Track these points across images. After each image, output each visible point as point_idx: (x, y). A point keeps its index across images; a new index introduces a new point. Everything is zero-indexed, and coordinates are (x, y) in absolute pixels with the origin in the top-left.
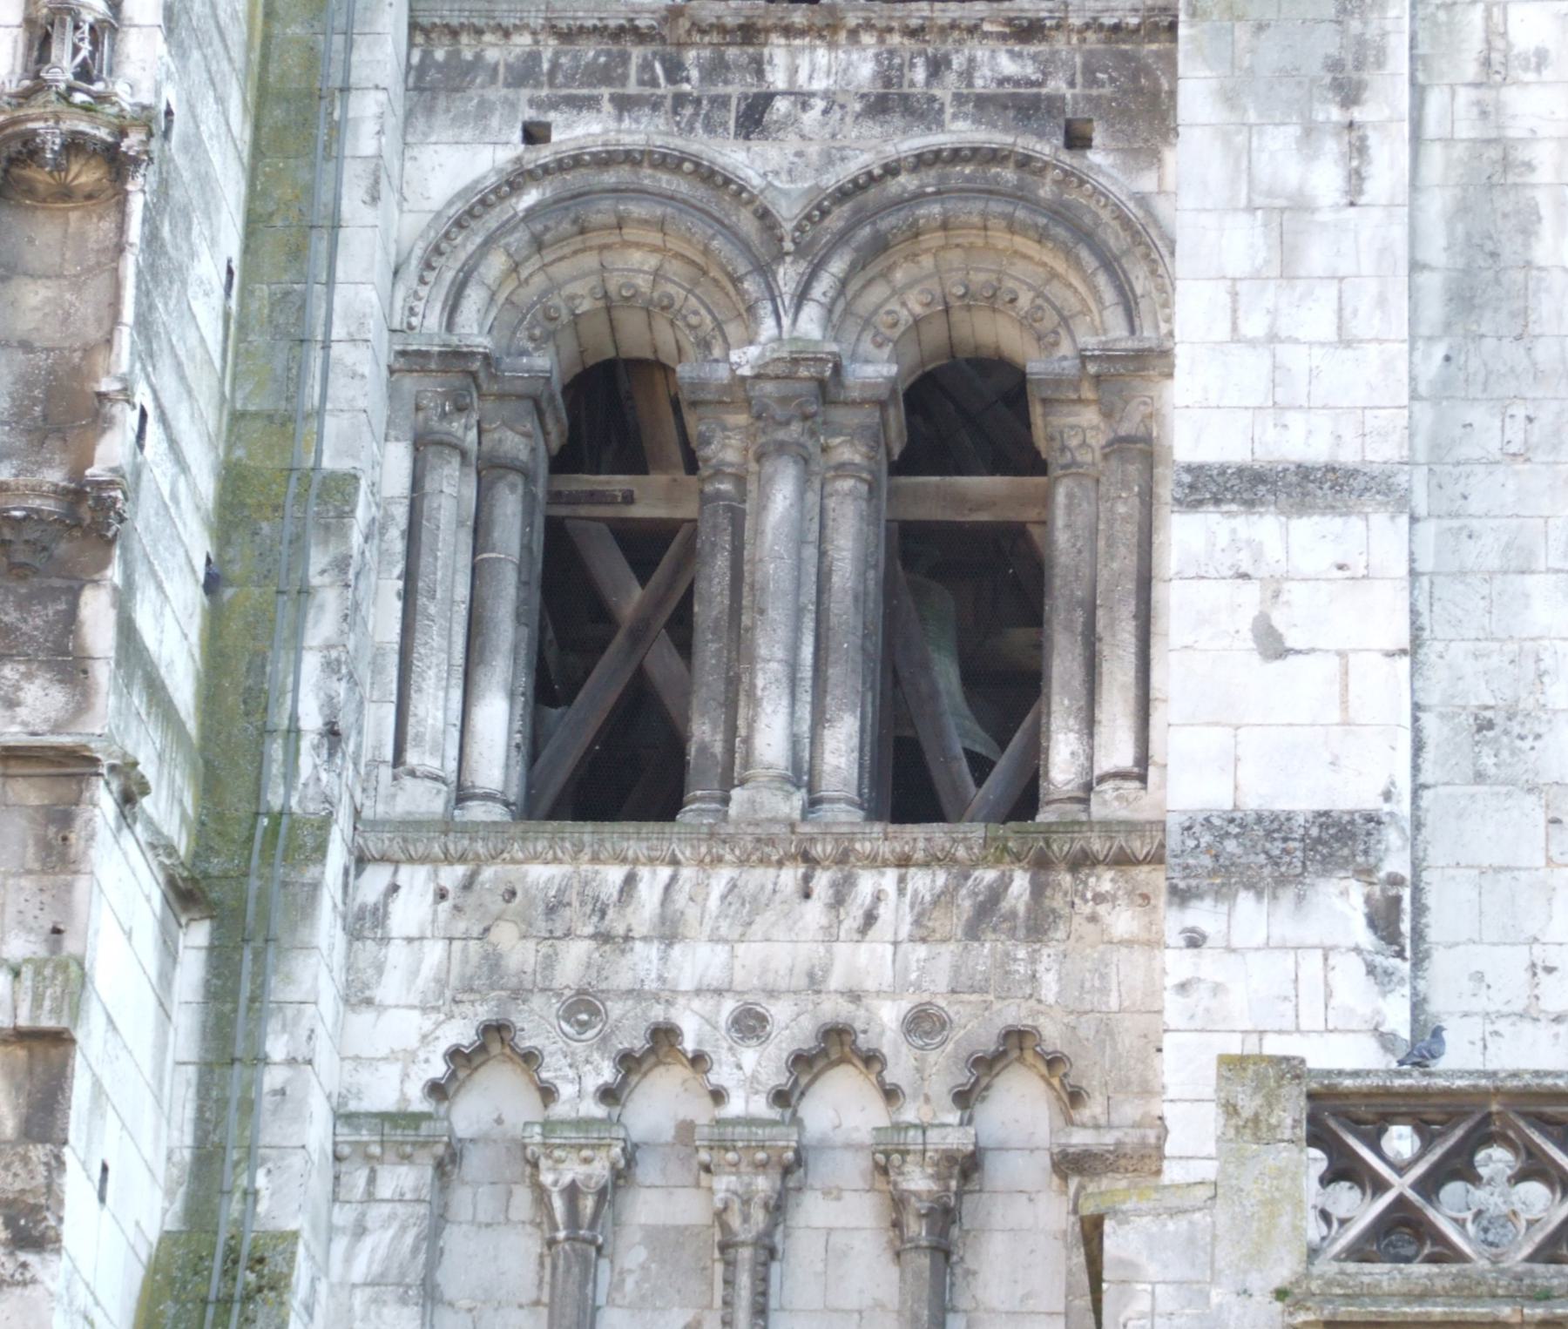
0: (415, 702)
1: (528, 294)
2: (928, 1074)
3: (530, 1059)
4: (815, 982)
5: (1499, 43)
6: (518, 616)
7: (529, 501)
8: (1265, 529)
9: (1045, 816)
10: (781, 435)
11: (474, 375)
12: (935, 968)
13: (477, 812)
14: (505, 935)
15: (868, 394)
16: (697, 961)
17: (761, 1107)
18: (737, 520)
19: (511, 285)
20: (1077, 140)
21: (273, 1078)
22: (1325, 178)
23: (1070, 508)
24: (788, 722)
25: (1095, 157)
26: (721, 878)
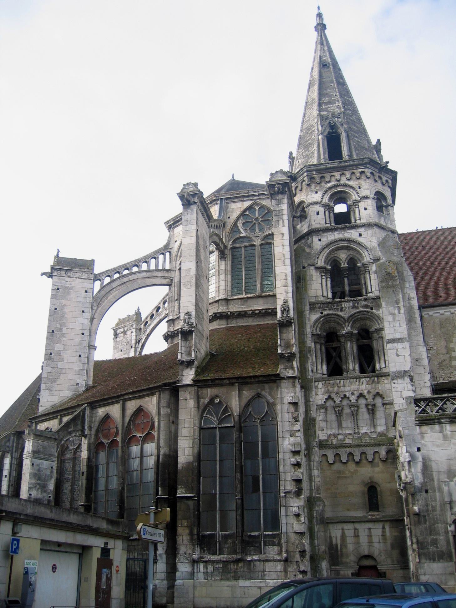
0: (318, 367)
3: (348, 398)
4: (358, 389)
8: (395, 345)
9: (377, 372)
12: (369, 387)
13: (324, 376)
14: (329, 387)
16: (348, 388)
17: (355, 401)
18: (345, 347)
20: (372, 309)
21: (311, 403)
22: (396, 311)
24: (353, 366)
25: (374, 311)
26: (348, 381)
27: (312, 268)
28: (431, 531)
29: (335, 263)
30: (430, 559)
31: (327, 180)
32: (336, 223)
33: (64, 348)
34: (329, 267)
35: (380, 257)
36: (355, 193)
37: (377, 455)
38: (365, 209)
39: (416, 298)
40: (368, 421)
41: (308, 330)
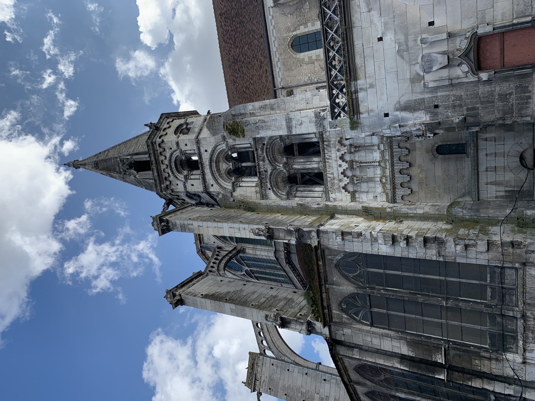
0: (314, 197)
2: (344, 150)
3: (345, 185)
7: (299, 187)
12: (333, 150)
16: (335, 171)
20: (264, 144)
24: (314, 164)
25: (265, 143)
26: (328, 170)
28: (488, 102)
29: (229, 173)
30: (527, 103)
31: (167, 175)
32: (199, 169)
33: (318, 394)
34: (233, 179)
36: (175, 153)
37: (402, 145)
40: (367, 151)
41: (284, 203)
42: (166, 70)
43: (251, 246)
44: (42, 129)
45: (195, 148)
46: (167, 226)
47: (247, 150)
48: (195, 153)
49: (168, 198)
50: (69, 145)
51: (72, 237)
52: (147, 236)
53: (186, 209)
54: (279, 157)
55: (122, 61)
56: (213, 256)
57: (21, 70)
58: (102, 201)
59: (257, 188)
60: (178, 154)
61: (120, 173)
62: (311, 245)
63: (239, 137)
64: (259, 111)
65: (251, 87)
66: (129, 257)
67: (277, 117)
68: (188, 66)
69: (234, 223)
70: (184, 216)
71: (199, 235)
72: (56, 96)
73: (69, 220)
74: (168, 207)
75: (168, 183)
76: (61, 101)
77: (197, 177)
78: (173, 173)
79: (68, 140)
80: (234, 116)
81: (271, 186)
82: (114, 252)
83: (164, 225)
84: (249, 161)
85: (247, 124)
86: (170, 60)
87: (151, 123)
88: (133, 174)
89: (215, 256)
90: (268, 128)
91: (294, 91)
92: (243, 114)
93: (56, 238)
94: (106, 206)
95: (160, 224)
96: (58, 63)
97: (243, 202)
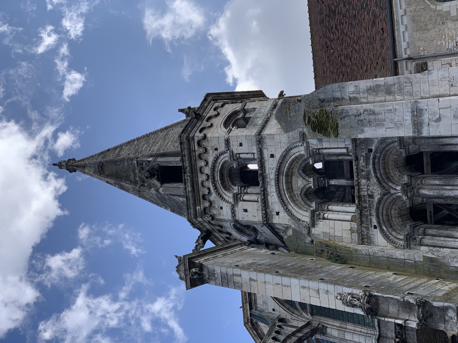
1: (399, 228)
5: (354, 92)
6: (447, 230)
7: (430, 228)
10: (416, 192)
11: (410, 237)
15: (409, 179)
19: (398, 231)
20: (370, 151)
23: (424, 149)
27: (313, 231)
29: (308, 195)
31: (206, 192)
32: (257, 184)
34: (314, 205)
35: (300, 132)
38: (241, 145)
39: (356, 83)
41: (399, 254)
42: (220, 29)
43: (337, 323)
44: (29, 112)
45: (255, 151)
46: (199, 275)
47: (341, 158)
48: (254, 159)
49: (205, 229)
50: (65, 140)
51: (55, 282)
52: (169, 290)
53: (232, 250)
54: (395, 174)
55: (154, 15)
56: (270, 333)
57: (10, 25)
58: (105, 229)
59: (353, 223)
60: (227, 159)
61: (136, 183)
62: (445, 334)
63: (329, 136)
64: (366, 95)
65: (355, 55)
66: (138, 322)
67: (397, 107)
68: (255, 23)
69: (310, 279)
70: (229, 260)
71: (250, 294)
72: (56, 64)
73: (53, 255)
74: (204, 242)
75: (207, 204)
76: (61, 73)
77: (254, 197)
78: (216, 188)
79: (64, 132)
80: (322, 101)
81: (379, 222)
82: (116, 312)
83: (196, 273)
84: (342, 176)
85: (344, 115)
86: (228, 14)
87: (189, 108)
88: (155, 186)
89: (274, 334)
90: (380, 124)
91: (429, 64)
92: (338, 99)
93: (32, 282)
94: (110, 237)
95: (190, 269)
96: (63, 17)
97: (327, 246)
